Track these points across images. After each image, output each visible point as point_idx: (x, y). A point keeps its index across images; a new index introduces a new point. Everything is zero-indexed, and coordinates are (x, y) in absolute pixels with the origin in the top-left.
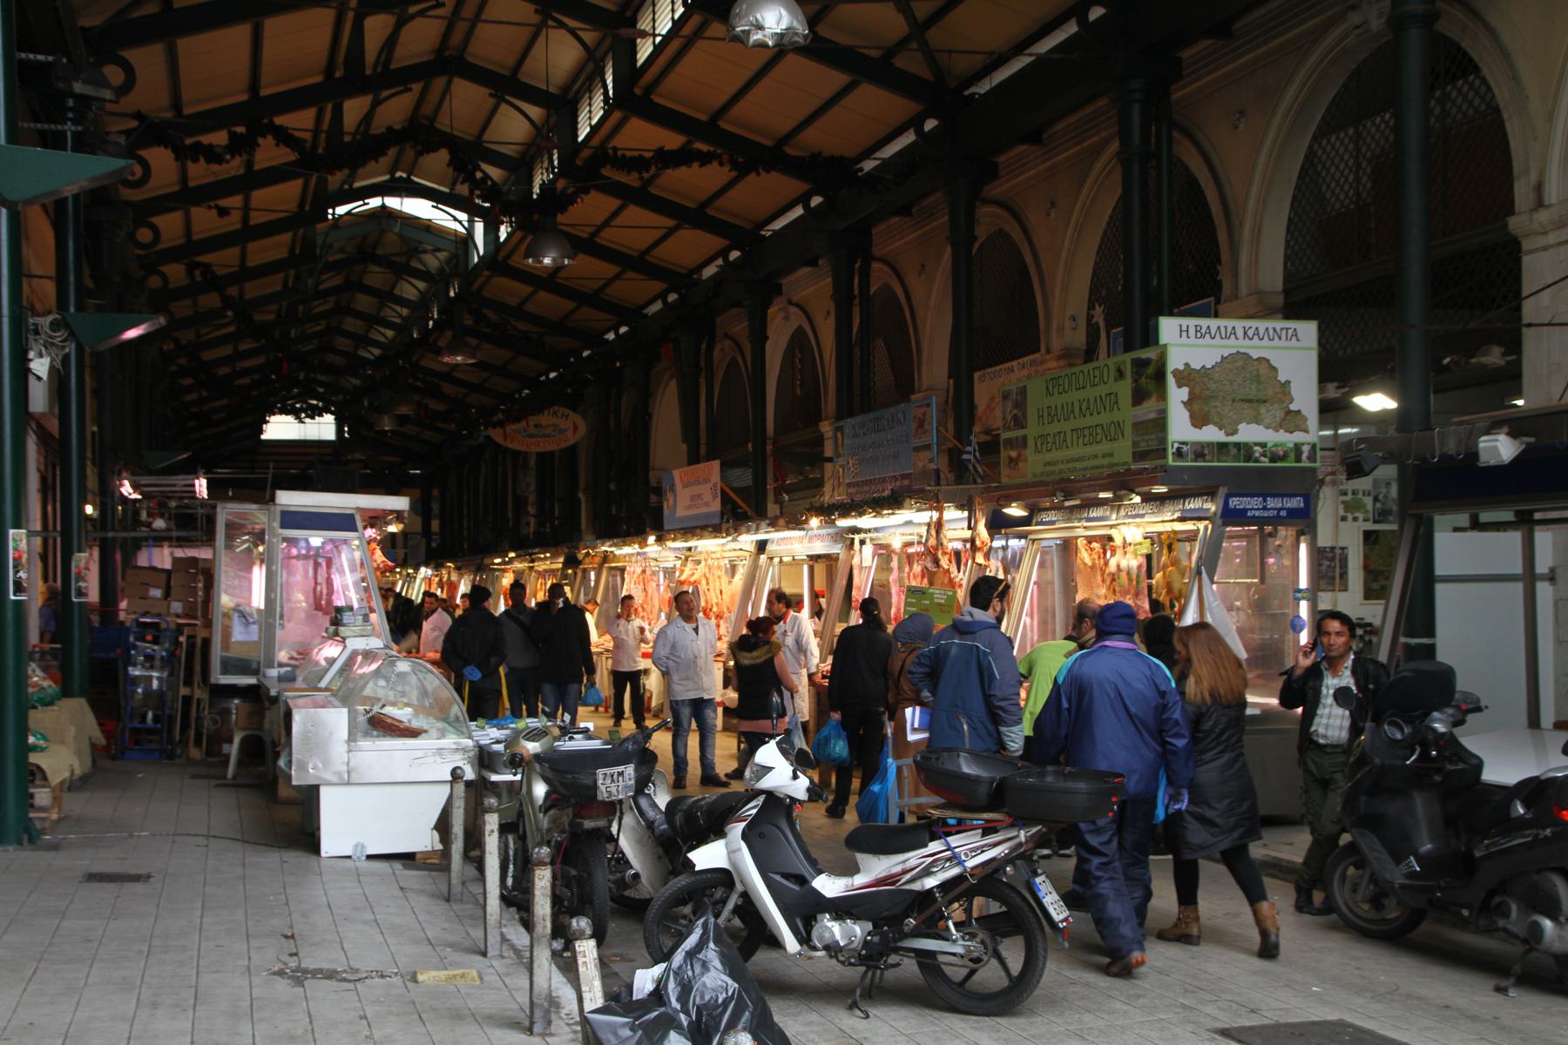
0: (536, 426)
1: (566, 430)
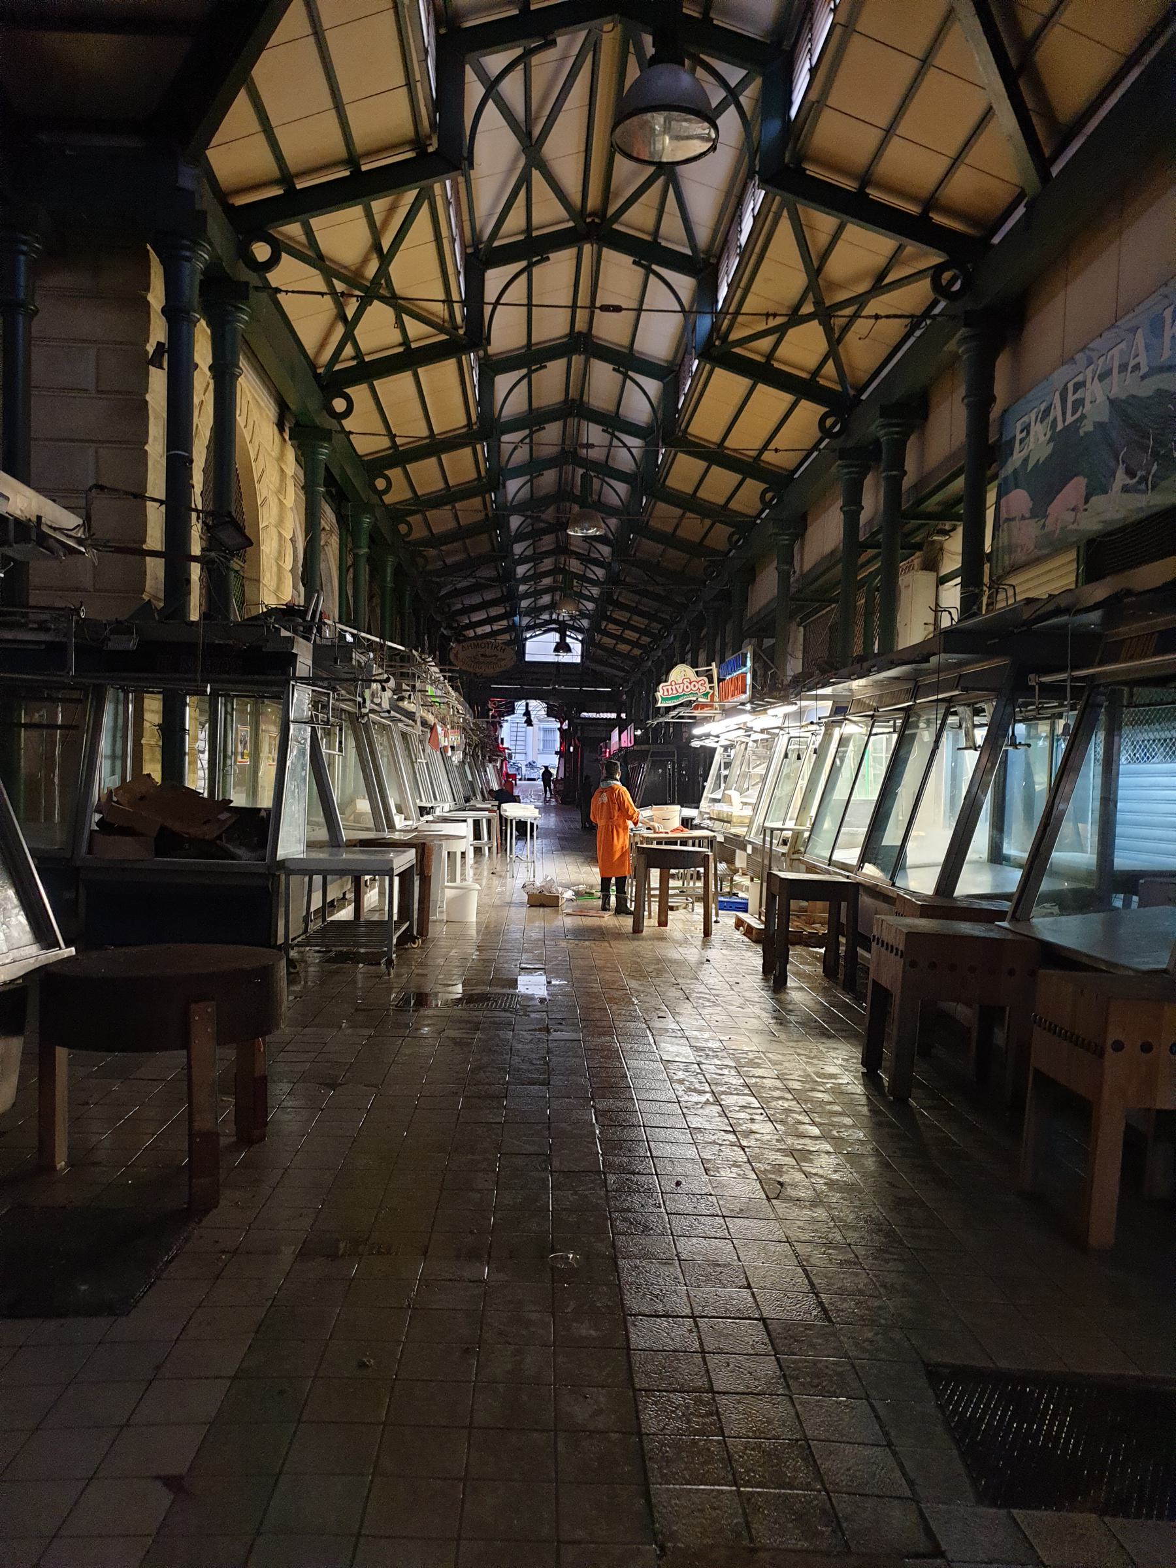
0: (482, 655)
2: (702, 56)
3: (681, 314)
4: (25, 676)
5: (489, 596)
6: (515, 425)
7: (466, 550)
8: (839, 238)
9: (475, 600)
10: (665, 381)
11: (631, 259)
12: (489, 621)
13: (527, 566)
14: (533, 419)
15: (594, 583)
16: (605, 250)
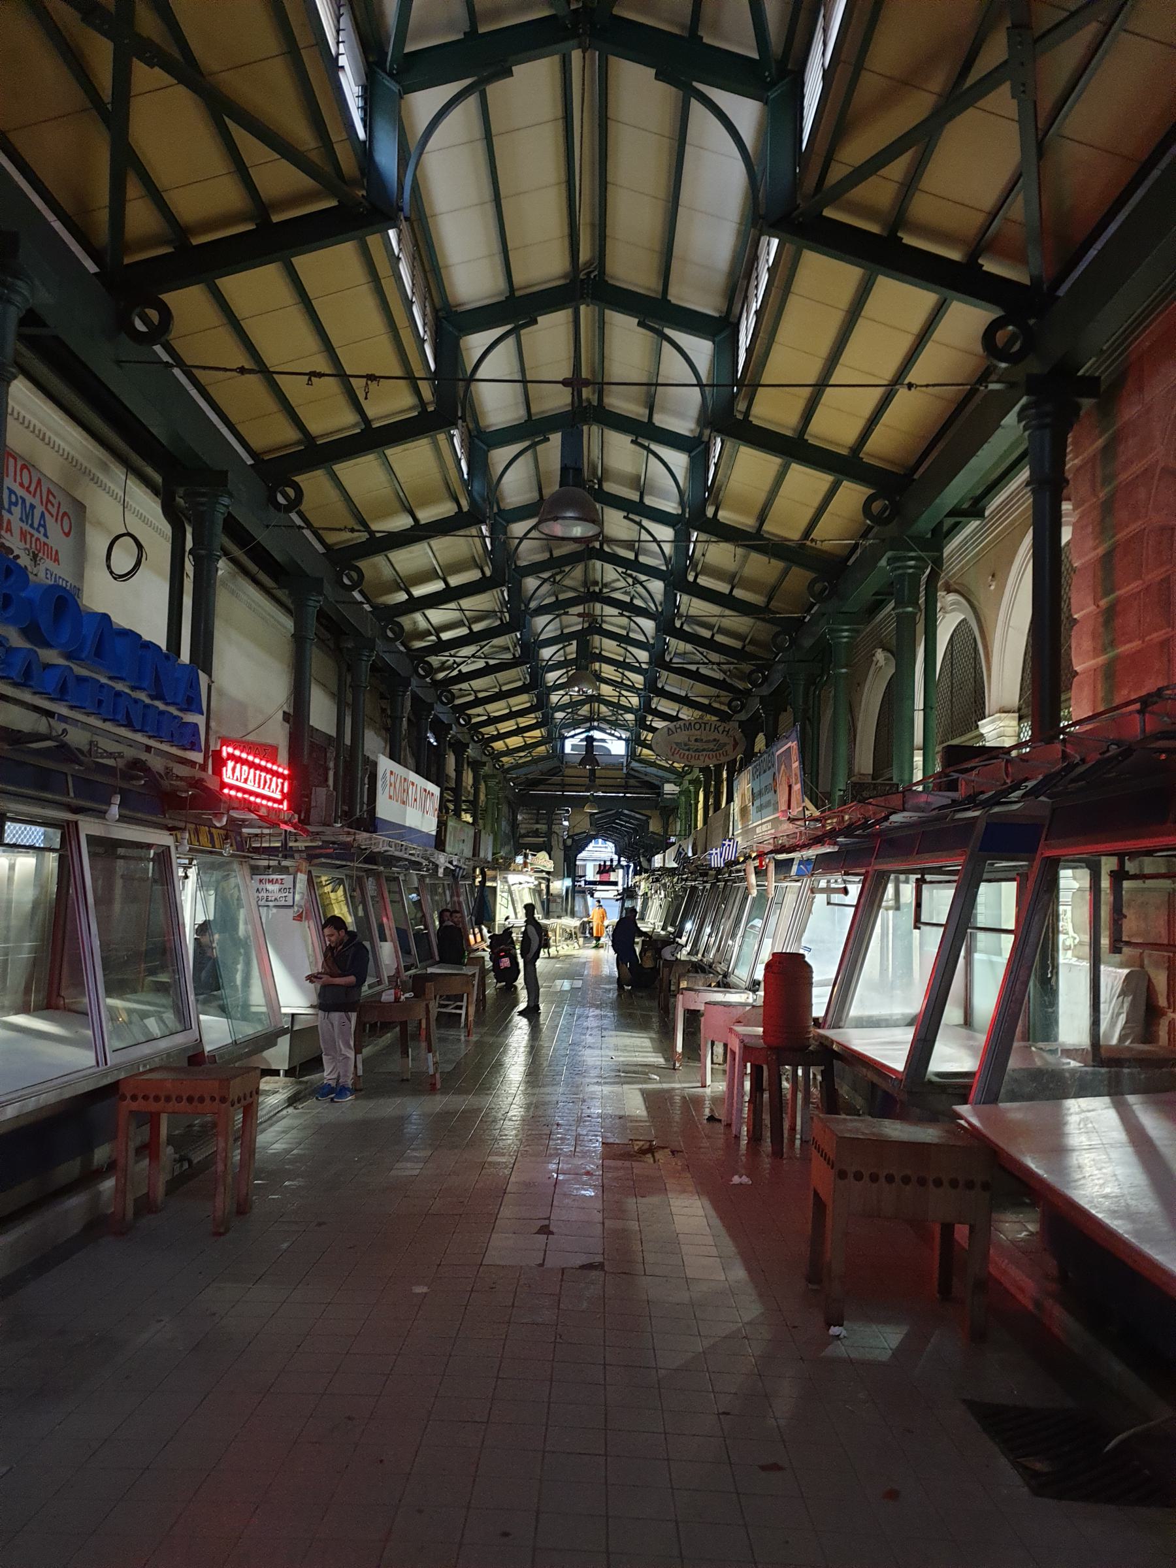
1: (725, 744)
2: (695, 84)
3: (697, 389)
4: (890, 970)
5: (524, 722)
6: (534, 569)
7: (517, 724)
8: (827, 360)
9: (509, 726)
10: (693, 454)
11: (636, 321)
12: (519, 731)
13: (554, 649)
14: (553, 565)
15: (628, 710)
16: (613, 59)
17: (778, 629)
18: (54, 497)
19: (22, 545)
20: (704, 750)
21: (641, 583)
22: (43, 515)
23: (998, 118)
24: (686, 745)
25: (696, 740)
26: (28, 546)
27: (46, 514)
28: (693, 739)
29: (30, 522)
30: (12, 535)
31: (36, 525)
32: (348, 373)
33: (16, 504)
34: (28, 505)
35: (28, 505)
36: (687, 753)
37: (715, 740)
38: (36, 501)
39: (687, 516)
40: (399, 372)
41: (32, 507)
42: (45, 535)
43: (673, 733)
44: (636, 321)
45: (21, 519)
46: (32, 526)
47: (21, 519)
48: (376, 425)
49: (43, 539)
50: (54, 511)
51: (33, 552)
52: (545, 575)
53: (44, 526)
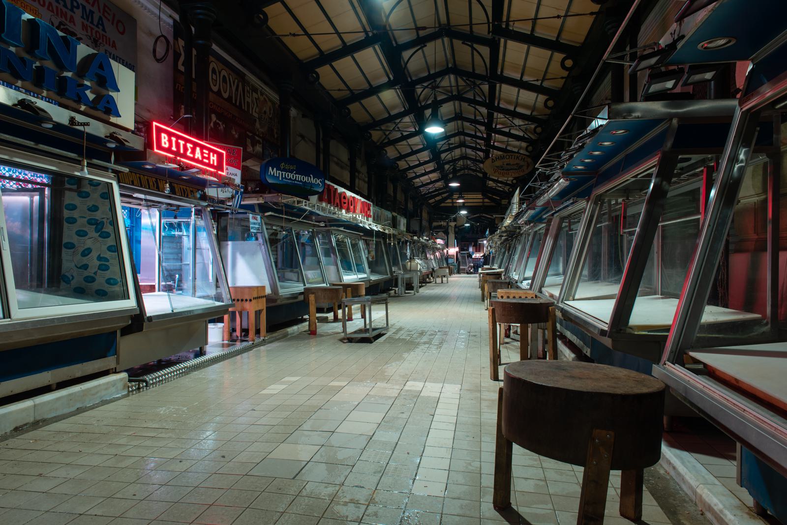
1: (522, 166)
11: (461, 42)
17: (528, 144)
18: (110, 10)
19: (85, 33)
20: (511, 169)
21: (477, 165)
22: (100, 18)
23: (427, 442)
24: (502, 167)
25: (507, 164)
26: (89, 34)
27: (103, 18)
28: (505, 163)
29: (90, 20)
30: (75, 25)
31: (95, 23)
32: (340, 32)
33: (78, 7)
34: (88, 11)
35: (88, 11)
36: (502, 171)
37: (517, 164)
38: (95, 9)
39: (487, 101)
40: (362, 30)
41: (92, 12)
42: (104, 30)
43: (495, 161)
44: (461, 42)
45: (82, 17)
46: (92, 23)
47: (82, 17)
48: (348, 44)
49: (102, 32)
50: (110, 18)
51: (94, 39)
52: (425, 84)
53: (103, 25)
